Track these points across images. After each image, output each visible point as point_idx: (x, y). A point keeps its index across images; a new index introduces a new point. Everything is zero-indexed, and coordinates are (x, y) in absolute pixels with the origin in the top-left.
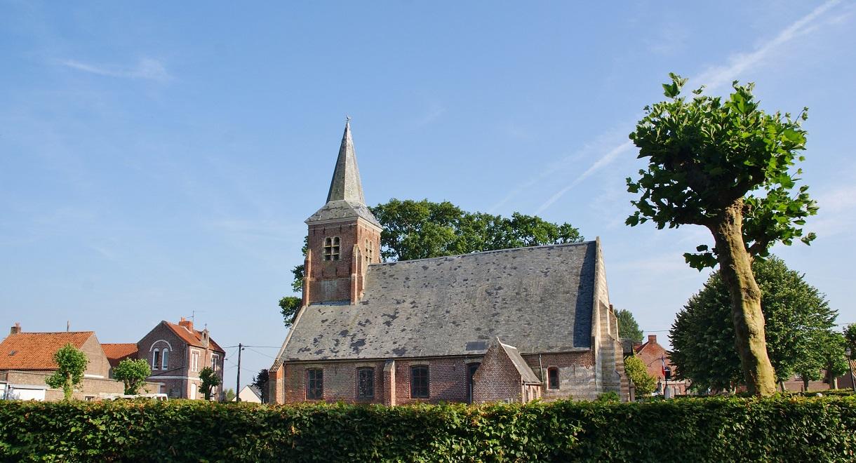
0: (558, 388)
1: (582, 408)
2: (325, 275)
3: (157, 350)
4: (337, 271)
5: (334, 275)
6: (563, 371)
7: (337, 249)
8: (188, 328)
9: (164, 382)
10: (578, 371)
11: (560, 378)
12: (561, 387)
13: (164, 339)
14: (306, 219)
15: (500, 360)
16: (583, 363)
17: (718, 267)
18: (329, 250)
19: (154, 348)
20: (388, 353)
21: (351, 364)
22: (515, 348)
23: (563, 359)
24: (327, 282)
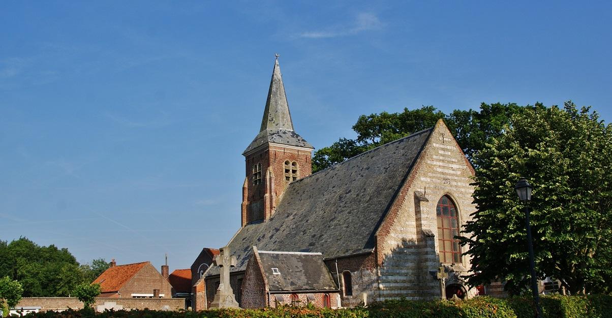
14: (243, 152)
19: (199, 272)
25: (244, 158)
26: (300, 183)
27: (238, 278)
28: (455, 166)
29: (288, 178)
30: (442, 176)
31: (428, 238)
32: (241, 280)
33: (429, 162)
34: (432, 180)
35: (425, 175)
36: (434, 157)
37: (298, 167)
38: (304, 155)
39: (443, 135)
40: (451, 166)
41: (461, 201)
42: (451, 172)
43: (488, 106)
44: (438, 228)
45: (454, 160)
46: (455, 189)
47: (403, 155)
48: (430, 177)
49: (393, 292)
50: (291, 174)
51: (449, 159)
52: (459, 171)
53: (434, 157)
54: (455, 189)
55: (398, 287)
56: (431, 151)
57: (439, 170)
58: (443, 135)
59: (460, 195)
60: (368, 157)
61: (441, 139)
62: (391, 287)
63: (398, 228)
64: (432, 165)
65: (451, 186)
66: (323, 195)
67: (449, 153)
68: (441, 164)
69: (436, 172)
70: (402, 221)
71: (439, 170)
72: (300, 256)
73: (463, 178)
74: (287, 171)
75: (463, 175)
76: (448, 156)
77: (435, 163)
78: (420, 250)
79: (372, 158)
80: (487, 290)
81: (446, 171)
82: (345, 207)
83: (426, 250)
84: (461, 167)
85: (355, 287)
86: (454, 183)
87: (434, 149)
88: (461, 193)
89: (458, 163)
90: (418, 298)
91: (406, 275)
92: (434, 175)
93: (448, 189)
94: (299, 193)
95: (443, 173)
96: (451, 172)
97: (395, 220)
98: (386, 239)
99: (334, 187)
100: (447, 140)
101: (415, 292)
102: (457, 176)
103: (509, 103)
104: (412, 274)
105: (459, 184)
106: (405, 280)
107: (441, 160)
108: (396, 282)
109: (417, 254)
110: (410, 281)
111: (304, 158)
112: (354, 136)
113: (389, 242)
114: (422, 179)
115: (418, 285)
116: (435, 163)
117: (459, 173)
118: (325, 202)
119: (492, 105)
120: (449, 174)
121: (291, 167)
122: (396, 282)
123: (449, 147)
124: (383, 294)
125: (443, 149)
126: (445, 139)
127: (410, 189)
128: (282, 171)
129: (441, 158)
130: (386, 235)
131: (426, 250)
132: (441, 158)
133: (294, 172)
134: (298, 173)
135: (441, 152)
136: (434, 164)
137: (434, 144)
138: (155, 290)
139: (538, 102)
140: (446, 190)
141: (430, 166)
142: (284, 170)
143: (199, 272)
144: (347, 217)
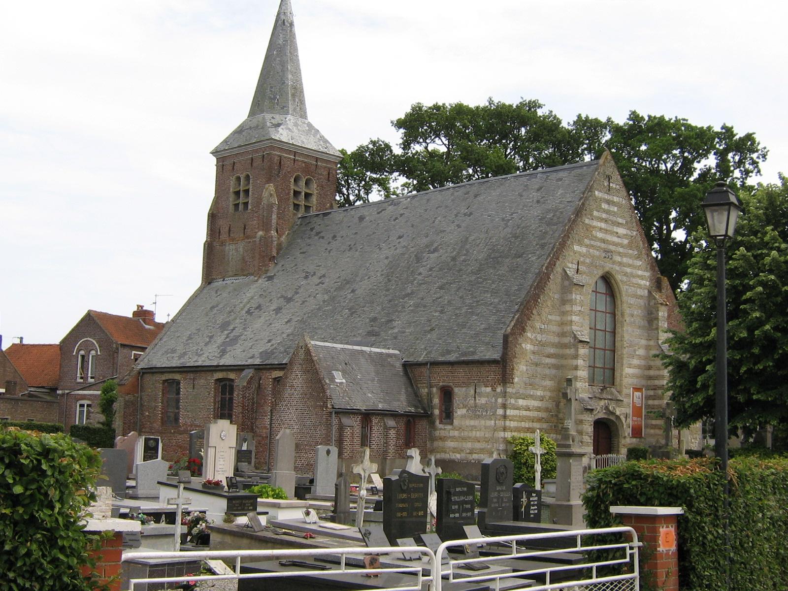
0: (452, 424)
1: (31, 503)
2: (232, 235)
3: (82, 352)
4: (245, 228)
5: (242, 235)
6: (459, 392)
7: (247, 192)
8: (144, 321)
9: (89, 399)
10: (481, 395)
11: (455, 405)
12: (456, 422)
13: (84, 337)
14: (212, 148)
15: (306, 371)
16: (488, 381)
17: (398, 151)
18: (237, 193)
19: (78, 353)
20: (252, 357)
21: (209, 374)
22: (397, 352)
23: (461, 372)
24: (232, 247)
25: (214, 160)
26: (323, 220)
27: (273, 377)
28: (621, 231)
29: (296, 207)
30: (603, 245)
31: (580, 345)
32: (279, 380)
33: (587, 221)
34: (589, 251)
35: (580, 243)
36: (595, 213)
37: (314, 188)
38: (325, 167)
39: (609, 178)
40: (616, 229)
41: (625, 287)
42: (616, 239)
43: (642, 117)
44: (590, 328)
45: (620, 220)
46: (617, 268)
47: (538, 202)
48: (587, 246)
49: (523, 424)
50: (302, 201)
51: (615, 219)
52: (626, 238)
53: (595, 213)
54: (617, 268)
55: (530, 417)
56: (592, 203)
57: (600, 235)
58: (609, 178)
59: (625, 279)
60: (467, 193)
61: (606, 184)
62: (520, 416)
63: (538, 325)
64: (591, 226)
65: (614, 263)
66: (380, 249)
67: (616, 209)
68: (603, 225)
69: (595, 238)
70: (543, 313)
71: (600, 235)
72: (370, 354)
73: (631, 252)
74: (296, 194)
75: (630, 246)
76: (615, 214)
77: (595, 223)
78: (564, 362)
79: (476, 196)
80: (645, 431)
81: (609, 238)
82: (431, 275)
83: (574, 362)
84: (629, 233)
85: (459, 412)
86: (618, 258)
87: (596, 199)
88: (626, 274)
89: (625, 225)
90: (555, 435)
91: (542, 399)
92: (592, 242)
93: (608, 267)
94: (323, 238)
95: (604, 241)
96: (616, 239)
97: (534, 312)
98: (520, 340)
99: (400, 237)
100: (614, 186)
101: (551, 426)
102: (622, 246)
103: (676, 117)
104: (550, 397)
105: (625, 260)
106: (540, 408)
107: (603, 219)
108: (528, 409)
109: (557, 367)
110: (547, 410)
111: (326, 173)
112: (395, 139)
113: (523, 345)
114: (576, 248)
115: (556, 416)
116: (595, 223)
117: (626, 242)
118: (386, 262)
119: (649, 117)
120: (613, 242)
121: (302, 187)
122: (528, 409)
123: (616, 199)
124: (510, 427)
125: (608, 202)
126: (611, 185)
127: (558, 263)
128: (289, 194)
129: (604, 216)
130: (521, 334)
131: (574, 362)
132: (604, 216)
133: (307, 196)
134: (314, 199)
135: (604, 206)
136: (594, 224)
137: (596, 193)
138: (8, 382)
139: (725, 124)
140: (607, 269)
141: (589, 228)
142: (292, 191)
143: (78, 353)
144: (438, 295)
